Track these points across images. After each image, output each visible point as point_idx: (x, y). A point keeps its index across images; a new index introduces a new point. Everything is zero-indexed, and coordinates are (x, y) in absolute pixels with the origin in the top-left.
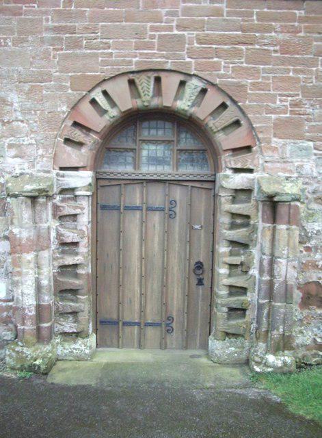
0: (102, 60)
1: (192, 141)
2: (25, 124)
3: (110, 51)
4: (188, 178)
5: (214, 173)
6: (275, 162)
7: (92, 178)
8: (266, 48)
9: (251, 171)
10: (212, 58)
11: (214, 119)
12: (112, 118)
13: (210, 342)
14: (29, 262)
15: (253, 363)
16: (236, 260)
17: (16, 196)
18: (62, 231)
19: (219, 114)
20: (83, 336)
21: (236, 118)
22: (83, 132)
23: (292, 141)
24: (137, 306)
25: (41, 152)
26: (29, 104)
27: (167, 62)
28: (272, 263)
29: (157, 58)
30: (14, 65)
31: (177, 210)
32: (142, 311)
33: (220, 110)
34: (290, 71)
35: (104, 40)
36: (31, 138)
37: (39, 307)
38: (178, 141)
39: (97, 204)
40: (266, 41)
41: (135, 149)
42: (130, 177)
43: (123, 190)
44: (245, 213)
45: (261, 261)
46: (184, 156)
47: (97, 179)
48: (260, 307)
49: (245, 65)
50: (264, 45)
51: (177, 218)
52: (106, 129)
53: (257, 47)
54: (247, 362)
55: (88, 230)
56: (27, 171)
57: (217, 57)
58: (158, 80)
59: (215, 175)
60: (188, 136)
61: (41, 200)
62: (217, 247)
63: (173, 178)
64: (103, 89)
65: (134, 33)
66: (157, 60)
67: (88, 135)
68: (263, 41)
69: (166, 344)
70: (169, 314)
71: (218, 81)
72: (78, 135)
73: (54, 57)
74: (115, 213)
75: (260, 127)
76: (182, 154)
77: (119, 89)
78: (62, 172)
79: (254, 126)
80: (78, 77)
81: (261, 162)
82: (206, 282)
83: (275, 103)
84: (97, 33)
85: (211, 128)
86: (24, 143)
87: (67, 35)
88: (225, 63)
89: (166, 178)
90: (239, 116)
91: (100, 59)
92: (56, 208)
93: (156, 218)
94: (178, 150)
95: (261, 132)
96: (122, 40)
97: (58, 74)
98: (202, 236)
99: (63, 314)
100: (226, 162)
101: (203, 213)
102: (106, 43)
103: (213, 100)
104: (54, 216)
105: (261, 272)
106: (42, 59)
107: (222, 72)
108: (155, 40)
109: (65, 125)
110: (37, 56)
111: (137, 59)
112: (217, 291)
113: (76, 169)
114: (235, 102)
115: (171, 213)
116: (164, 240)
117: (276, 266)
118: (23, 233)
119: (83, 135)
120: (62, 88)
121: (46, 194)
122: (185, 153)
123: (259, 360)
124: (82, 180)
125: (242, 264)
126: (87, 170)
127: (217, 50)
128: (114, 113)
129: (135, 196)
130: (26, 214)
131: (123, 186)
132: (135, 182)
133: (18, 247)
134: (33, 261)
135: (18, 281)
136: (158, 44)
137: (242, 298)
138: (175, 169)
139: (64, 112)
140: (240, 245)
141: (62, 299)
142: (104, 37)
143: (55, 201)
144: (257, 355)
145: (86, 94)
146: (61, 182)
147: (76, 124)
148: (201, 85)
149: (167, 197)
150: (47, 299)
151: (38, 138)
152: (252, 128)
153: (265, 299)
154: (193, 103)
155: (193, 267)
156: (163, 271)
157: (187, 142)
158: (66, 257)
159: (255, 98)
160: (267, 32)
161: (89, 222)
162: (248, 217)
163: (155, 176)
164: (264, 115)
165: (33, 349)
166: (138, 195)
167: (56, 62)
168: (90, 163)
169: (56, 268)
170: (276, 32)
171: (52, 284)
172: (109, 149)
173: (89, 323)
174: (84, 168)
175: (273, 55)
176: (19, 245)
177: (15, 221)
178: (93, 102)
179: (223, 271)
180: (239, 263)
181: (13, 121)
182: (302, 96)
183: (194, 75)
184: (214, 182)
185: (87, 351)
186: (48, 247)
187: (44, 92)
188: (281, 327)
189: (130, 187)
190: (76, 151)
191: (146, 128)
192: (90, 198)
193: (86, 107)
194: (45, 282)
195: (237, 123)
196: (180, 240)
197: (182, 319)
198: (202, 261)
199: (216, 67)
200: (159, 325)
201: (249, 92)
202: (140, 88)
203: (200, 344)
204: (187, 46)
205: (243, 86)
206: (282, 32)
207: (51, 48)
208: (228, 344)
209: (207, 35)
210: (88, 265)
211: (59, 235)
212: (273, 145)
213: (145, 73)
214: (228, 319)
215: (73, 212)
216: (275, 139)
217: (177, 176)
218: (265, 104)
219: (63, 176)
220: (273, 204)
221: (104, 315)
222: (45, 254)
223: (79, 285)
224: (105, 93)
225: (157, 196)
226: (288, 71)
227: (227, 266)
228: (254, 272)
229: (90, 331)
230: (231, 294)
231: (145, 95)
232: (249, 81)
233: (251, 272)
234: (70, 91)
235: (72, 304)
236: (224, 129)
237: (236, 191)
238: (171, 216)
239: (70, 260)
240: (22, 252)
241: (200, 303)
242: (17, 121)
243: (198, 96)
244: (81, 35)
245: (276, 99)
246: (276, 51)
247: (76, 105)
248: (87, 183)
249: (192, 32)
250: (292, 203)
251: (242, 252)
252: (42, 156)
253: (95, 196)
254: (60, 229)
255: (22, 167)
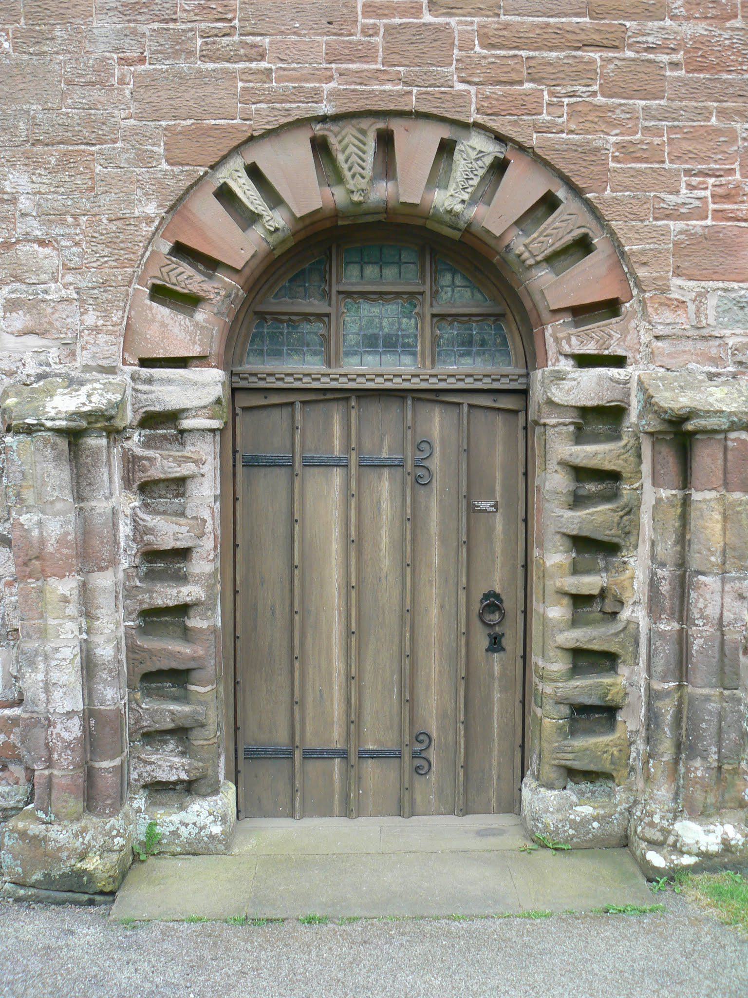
0: (244, 89)
1: (467, 293)
2: (47, 251)
3: (264, 65)
4: (460, 385)
5: (523, 371)
6: (679, 337)
7: (223, 384)
8: (651, 56)
9: (619, 362)
10: (521, 83)
11: (527, 234)
12: (271, 233)
13: (526, 794)
14: (65, 600)
15: (644, 845)
16: (590, 583)
17: (29, 430)
18: (151, 520)
19: (539, 221)
20: (203, 790)
21: (583, 230)
22: (199, 271)
23: (720, 284)
24: (337, 709)
25: (91, 318)
26: (58, 201)
27: (410, 93)
28: (683, 585)
29: (382, 82)
30: (14, 100)
31: (435, 464)
32: (353, 721)
33: (540, 212)
34: (711, 113)
35: (250, 39)
36: (66, 286)
37: (89, 714)
38: (435, 294)
39: (235, 452)
40: (650, 39)
41: (328, 315)
42: (316, 385)
43: (298, 416)
44: (608, 466)
45: (653, 585)
46: (450, 332)
47: (234, 391)
48: (652, 696)
49: (600, 100)
50: (648, 49)
51: (436, 485)
52: (255, 262)
53: (630, 54)
54: (625, 842)
55: (213, 516)
56: (56, 368)
57: (532, 80)
58: (386, 140)
59: (527, 375)
60: (458, 281)
61: (96, 442)
62: (536, 553)
63: (424, 385)
64: (249, 162)
65: (324, 21)
66: (386, 91)
67: (210, 277)
68: (644, 39)
69: (413, 801)
70: (418, 729)
71: (534, 140)
72: (186, 277)
73: (122, 81)
74: (281, 475)
75: (643, 252)
76: (444, 324)
77: (291, 164)
78: (145, 372)
79: (627, 248)
80: (186, 133)
81: (645, 338)
82: (512, 642)
83: (678, 192)
84: (230, 20)
85: (519, 256)
86: (48, 297)
87: (156, 26)
88: (552, 94)
89: (406, 385)
90: (589, 226)
91: (240, 84)
92: (131, 462)
93: (384, 488)
94: (433, 316)
95: (645, 264)
96: (294, 38)
97: (132, 122)
98: (499, 527)
99: (153, 737)
100: (557, 340)
101: (499, 476)
102: (253, 46)
103: (523, 187)
104: (127, 482)
105: (654, 606)
106: (92, 84)
107: (545, 117)
108: (378, 40)
109: (153, 252)
110: (80, 76)
111: (333, 85)
112: (541, 663)
113: (181, 362)
114: (577, 191)
115: (420, 472)
116: (403, 540)
117: (693, 595)
118: (50, 523)
119: (199, 277)
120: (144, 159)
121: (104, 422)
122: (451, 323)
123: (658, 836)
124: (199, 390)
125: (603, 593)
126: (209, 366)
127: (532, 63)
128: (276, 219)
129: (334, 429)
130: (55, 476)
131: (298, 406)
132: (329, 396)
133: (36, 563)
134: (75, 597)
135: (37, 653)
136: (385, 49)
137: (606, 680)
138: (428, 363)
139: (149, 220)
140: (591, 548)
141: (148, 693)
142: (249, 29)
143: (127, 444)
144: (652, 825)
145: (206, 173)
146: (143, 397)
147: (180, 250)
148: (492, 149)
149: (409, 432)
150: (111, 695)
151: (83, 284)
152: (620, 254)
153: (664, 679)
154: (473, 195)
155: (476, 607)
156: (402, 617)
157: (457, 295)
158: (158, 587)
159: (627, 181)
160: (651, 18)
161: (216, 497)
162: (614, 476)
163: (380, 380)
164: (650, 222)
165: (76, 827)
166: (337, 429)
167: (127, 92)
168: (215, 348)
169: (134, 616)
170: (673, 18)
171: (123, 657)
172: (262, 316)
173: (219, 756)
174: (201, 360)
175: (668, 73)
176: (37, 558)
177: (29, 496)
178: (225, 194)
179: (557, 612)
180: (596, 592)
181: (18, 241)
182: (742, 175)
183: (476, 125)
184: (524, 393)
185: (217, 829)
186: (113, 562)
187: (99, 169)
188: (714, 749)
189: (317, 411)
190: (181, 317)
191: (356, 263)
192: (218, 438)
193: (208, 211)
194: (105, 652)
195: (583, 246)
196: (443, 540)
197: (451, 737)
198: (498, 590)
199: (527, 107)
200: (397, 755)
201: (612, 165)
202: (341, 158)
203: (499, 803)
204: (456, 51)
205: (597, 150)
206: (687, 18)
207: (115, 56)
208: (574, 798)
209: (506, 26)
210: (215, 605)
211: (140, 531)
212: (674, 296)
213: (354, 122)
214: (573, 733)
215: (179, 471)
216: (677, 281)
217: (433, 380)
218: (652, 194)
219: (150, 381)
220: (680, 437)
221: (253, 735)
222: (105, 581)
223: (193, 659)
224: (254, 172)
225: (383, 433)
226: (706, 114)
227: (566, 601)
228: (635, 613)
229: (221, 777)
230: (575, 671)
231: (353, 176)
232: (613, 139)
233: (625, 614)
234: (165, 166)
235: (174, 707)
236: (550, 259)
237: (585, 412)
238: (420, 480)
239: (168, 595)
240: (43, 575)
241: (497, 695)
242: (29, 241)
243: (483, 179)
244: (190, 25)
245: (679, 181)
246: (675, 65)
247: (180, 199)
248: (212, 398)
249: (469, 19)
250: (733, 435)
251: (601, 564)
252: (96, 330)
253: (227, 435)
254: (144, 516)
255: (42, 357)
